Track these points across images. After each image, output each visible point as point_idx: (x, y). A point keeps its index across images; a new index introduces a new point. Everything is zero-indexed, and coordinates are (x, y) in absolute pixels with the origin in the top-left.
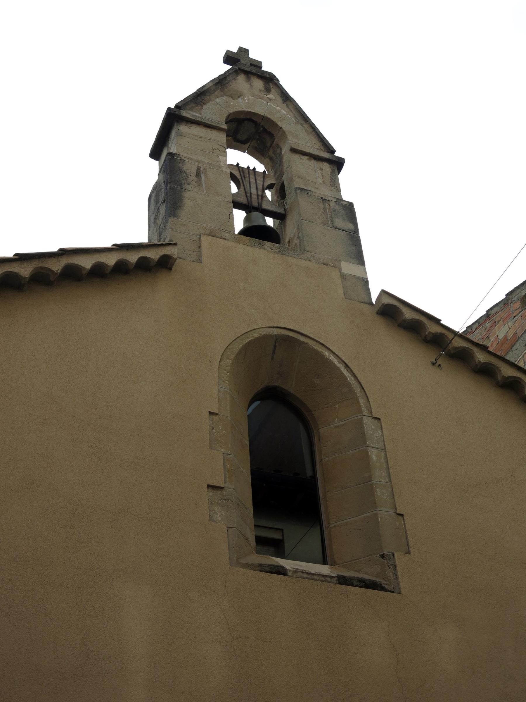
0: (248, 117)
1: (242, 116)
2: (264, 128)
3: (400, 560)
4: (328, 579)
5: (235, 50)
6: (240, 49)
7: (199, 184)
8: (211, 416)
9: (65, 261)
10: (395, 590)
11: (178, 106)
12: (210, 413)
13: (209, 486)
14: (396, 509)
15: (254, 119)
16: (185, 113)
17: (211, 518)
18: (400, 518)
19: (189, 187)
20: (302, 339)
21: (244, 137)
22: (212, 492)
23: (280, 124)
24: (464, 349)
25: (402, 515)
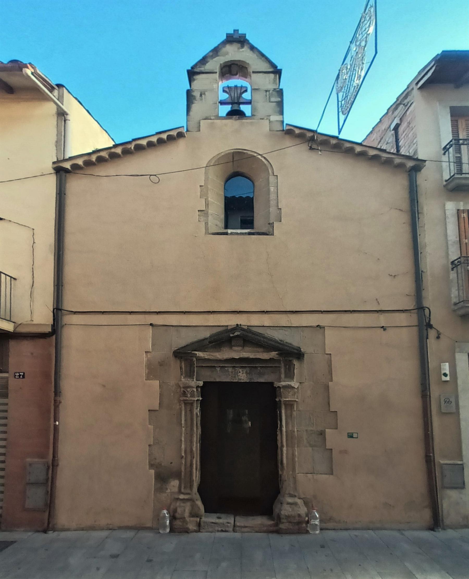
0: (232, 63)
1: (229, 64)
2: (242, 66)
3: (276, 225)
4: (244, 234)
5: (232, 32)
6: (234, 31)
7: (201, 100)
8: (201, 187)
9: (325, 138)
10: (273, 234)
11: (192, 68)
12: (200, 186)
13: (199, 211)
14: (278, 207)
15: (235, 63)
16: (197, 70)
17: (199, 221)
18: (280, 210)
19: (196, 102)
20: (245, 152)
21: (235, 73)
22: (200, 212)
23: (248, 62)
24: (326, 140)
25: (281, 209)
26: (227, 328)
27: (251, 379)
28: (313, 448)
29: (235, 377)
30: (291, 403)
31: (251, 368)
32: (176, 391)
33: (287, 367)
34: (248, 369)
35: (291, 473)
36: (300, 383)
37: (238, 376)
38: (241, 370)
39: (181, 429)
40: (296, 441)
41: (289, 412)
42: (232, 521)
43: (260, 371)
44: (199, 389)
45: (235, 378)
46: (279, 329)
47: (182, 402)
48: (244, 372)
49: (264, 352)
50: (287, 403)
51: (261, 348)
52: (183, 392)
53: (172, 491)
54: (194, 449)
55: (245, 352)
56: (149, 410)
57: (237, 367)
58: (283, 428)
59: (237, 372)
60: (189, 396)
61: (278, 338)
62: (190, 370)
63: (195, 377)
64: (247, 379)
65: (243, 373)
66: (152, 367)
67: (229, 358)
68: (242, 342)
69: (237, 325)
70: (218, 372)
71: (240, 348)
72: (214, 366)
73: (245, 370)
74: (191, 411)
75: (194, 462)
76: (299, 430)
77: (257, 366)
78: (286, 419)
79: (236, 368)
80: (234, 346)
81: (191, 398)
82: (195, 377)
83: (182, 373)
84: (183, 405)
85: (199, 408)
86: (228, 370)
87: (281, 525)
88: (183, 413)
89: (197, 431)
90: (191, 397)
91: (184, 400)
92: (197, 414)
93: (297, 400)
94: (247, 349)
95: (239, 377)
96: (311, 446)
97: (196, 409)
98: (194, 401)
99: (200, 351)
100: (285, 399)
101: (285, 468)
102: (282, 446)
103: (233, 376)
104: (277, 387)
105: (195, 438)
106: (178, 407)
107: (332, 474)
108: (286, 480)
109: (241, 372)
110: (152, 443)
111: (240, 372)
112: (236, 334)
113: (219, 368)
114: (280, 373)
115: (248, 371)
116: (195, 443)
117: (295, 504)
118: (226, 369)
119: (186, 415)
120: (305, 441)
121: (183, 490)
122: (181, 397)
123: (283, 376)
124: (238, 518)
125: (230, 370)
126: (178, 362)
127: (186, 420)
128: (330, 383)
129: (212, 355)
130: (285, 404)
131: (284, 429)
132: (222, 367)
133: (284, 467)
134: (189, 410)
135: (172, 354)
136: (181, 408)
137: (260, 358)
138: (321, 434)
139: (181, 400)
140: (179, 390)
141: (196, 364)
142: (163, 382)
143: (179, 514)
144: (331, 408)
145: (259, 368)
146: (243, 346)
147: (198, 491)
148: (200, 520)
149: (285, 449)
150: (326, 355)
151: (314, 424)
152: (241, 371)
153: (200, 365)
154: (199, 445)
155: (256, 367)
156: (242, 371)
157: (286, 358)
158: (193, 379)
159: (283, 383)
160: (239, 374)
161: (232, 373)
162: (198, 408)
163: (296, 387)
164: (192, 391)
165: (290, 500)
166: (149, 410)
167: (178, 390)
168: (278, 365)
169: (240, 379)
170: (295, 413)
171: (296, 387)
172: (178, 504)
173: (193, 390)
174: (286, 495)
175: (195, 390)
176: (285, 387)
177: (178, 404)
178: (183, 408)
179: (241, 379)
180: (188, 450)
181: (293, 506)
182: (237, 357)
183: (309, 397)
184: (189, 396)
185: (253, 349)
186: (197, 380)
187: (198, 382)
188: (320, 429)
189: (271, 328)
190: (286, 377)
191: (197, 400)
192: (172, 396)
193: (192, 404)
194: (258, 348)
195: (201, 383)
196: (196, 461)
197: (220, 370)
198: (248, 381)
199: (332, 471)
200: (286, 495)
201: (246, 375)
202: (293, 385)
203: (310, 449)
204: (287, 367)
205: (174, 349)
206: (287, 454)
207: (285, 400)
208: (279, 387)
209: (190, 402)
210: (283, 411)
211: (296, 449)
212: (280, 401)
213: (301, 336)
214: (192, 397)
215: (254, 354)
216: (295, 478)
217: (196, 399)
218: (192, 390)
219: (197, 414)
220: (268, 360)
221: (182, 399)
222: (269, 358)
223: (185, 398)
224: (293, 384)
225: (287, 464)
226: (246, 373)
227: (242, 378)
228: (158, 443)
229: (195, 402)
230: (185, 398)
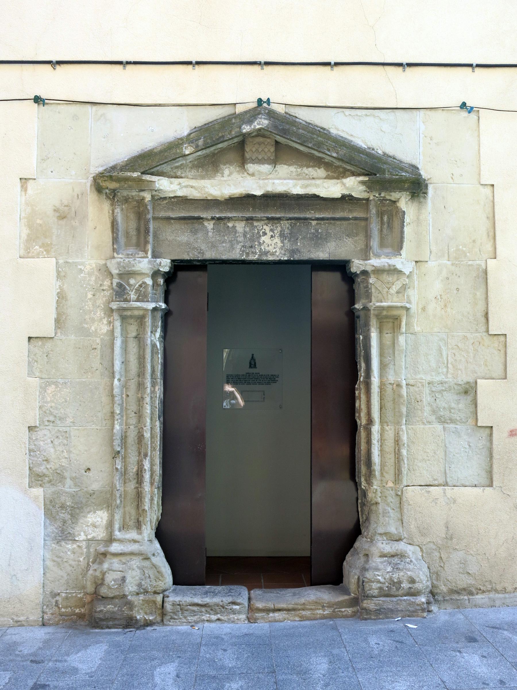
26: (232, 112)
27: (293, 252)
28: (446, 425)
29: (251, 247)
30: (395, 313)
31: (293, 221)
32: (101, 285)
33: (385, 218)
34: (286, 224)
35: (390, 484)
36: (416, 262)
37: (260, 244)
38: (267, 229)
39: (114, 422)
40: (404, 410)
41: (388, 337)
42: (243, 600)
43: (317, 231)
44: (161, 281)
45: (251, 250)
46: (366, 115)
47: (116, 316)
48: (277, 232)
49: (328, 177)
50: (385, 313)
51: (319, 168)
52: (117, 289)
53: (89, 537)
54: (147, 435)
55: (280, 179)
56: (30, 338)
57: (259, 220)
58: (372, 379)
59: (258, 233)
60: (133, 296)
61: (362, 141)
62: (138, 230)
63: (150, 247)
64: (283, 252)
65: (272, 236)
66: (39, 221)
67: (237, 196)
68: (273, 149)
69: (260, 101)
70: (210, 234)
71: (265, 168)
72: (199, 218)
73: (279, 229)
74: (139, 339)
75: (147, 465)
76: (412, 382)
77: (308, 216)
78: (382, 355)
79: (255, 224)
80: (254, 161)
81: (138, 304)
82: (150, 247)
83: (117, 234)
84: (118, 324)
85: (159, 330)
86: (234, 227)
87: (365, 601)
88: (118, 343)
89: (153, 392)
90: (138, 300)
91: (121, 310)
92: (154, 346)
93: (408, 305)
94: (283, 169)
95: (263, 248)
96: (441, 420)
97: (152, 332)
98: (146, 310)
99: (162, 176)
100: (378, 304)
101: (377, 473)
102: (370, 422)
103: (248, 244)
104: (358, 272)
105: (148, 407)
106: (105, 329)
107: (491, 485)
108: (377, 503)
109: (269, 234)
110: (38, 422)
111: (265, 234)
112: (258, 127)
113: (212, 223)
114: (368, 237)
115: (287, 231)
116: (148, 420)
117: (401, 555)
118: (230, 225)
119: (125, 349)
120: (427, 409)
121: (118, 534)
122: (112, 301)
123: (375, 243)
124: (256, 593)
125: (240, 227)
126: (106, 206)
127: (125, 363)
128: (491, 263)
129: (192, 187)
130: (377, 316)
131: (375, 380)
132: (220, 219)
133: (374, 470)
134: (134, 334)
135: (89, 185)
136: (112, 332)
137: (317, 193)
138: (466, 392)
139: (112, 310)
140: (107, 283)
141: (151, 211)
142: (67, 262)
143: (109, 588)
144: (490, 329)
145: (314, 223)
146: (275, 162)
147: (156, 537)
148: (163, 602)
149: (376, 429)
150: (481, 188)
151: (450, 366)
152: (268, 231)
153: (163, 214)
154: (158, 424)
155: (305, 219)
156: (272, 230)
157: (383, 195)
158: (146, 252)
159: (375, 262)
160: (263, 238)
161: (245, 236)
162: (156, 331)
163: (407, 273)
164: (141, 286)
165: (387, 547)
166: (30, 338)
167: (105, 283)
168: (361, 215)
169: (266, 253)
170: (402, 339)
171: (407, 273)
172: (106, 566)
173: (144, 283)
174: (378, 537)
175: (149, 281)
176: (379, 271)
177: (105, 321)
178: (118, 332)
179: (269, 252)
180: (132, 435)
181: (396, 560)
182: (258, 192)
183: (439, 297)
184: (133, 296)
185: (299, 170)
186: (155, 256)
187: (158, 260)
188: (464, 378)
189: (347, 112)
190: (382, 245)
191: (155, 309)
192: (90, 299)
193: (141, 319)
194: (312, 167)
195: (165, 265)
196: (152, 465)
197: (213, 229)
198: (286, 259)
199: (492, 482)
200: (378, 537)
201: (282, 242)
202: (399, 266)
203: (439, 427)
204: (385, 218)
205: (96, 168)
206: (382, 440)
207: (378, 307)
208: (365, 273)
209: (136, 313)
210: (374, 336)
211: (404, 427)
212: (366, 309)
213: (422, 136)
214: (143, 301)
215: (301, 182)
216: (400, 497)
217: (151, 306)
218: (140, 283)
219: (154, 346)
220: (337, 199)
221: (114, 306)
222: (339, 196)
223: (124, 305)
224: (397, 262)
225: (383, 465)
226: (282, 235)
227: (271, 249)
228: (53, 422)
229: (150, 313)
230: (124, 305)
